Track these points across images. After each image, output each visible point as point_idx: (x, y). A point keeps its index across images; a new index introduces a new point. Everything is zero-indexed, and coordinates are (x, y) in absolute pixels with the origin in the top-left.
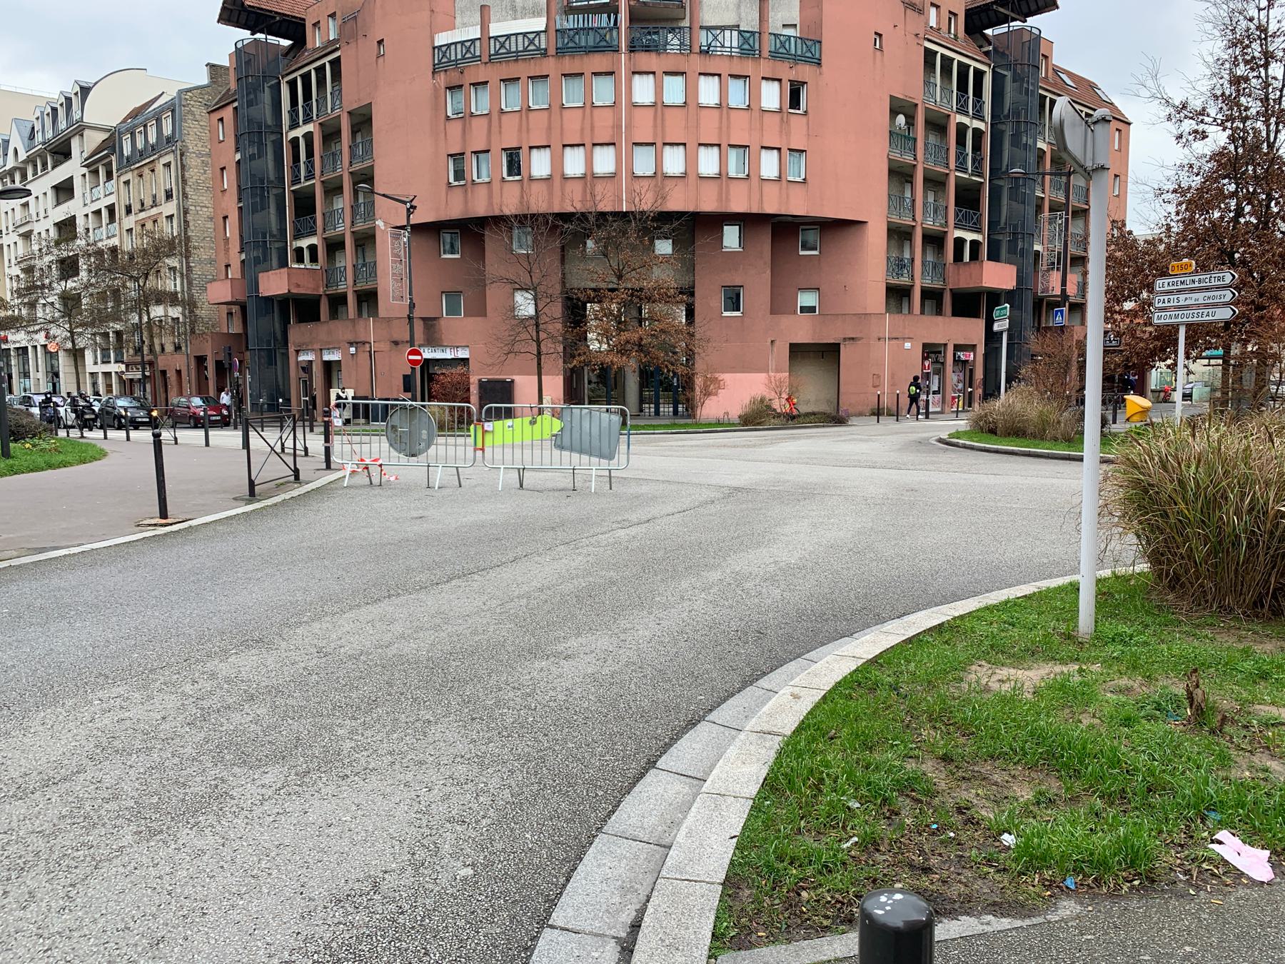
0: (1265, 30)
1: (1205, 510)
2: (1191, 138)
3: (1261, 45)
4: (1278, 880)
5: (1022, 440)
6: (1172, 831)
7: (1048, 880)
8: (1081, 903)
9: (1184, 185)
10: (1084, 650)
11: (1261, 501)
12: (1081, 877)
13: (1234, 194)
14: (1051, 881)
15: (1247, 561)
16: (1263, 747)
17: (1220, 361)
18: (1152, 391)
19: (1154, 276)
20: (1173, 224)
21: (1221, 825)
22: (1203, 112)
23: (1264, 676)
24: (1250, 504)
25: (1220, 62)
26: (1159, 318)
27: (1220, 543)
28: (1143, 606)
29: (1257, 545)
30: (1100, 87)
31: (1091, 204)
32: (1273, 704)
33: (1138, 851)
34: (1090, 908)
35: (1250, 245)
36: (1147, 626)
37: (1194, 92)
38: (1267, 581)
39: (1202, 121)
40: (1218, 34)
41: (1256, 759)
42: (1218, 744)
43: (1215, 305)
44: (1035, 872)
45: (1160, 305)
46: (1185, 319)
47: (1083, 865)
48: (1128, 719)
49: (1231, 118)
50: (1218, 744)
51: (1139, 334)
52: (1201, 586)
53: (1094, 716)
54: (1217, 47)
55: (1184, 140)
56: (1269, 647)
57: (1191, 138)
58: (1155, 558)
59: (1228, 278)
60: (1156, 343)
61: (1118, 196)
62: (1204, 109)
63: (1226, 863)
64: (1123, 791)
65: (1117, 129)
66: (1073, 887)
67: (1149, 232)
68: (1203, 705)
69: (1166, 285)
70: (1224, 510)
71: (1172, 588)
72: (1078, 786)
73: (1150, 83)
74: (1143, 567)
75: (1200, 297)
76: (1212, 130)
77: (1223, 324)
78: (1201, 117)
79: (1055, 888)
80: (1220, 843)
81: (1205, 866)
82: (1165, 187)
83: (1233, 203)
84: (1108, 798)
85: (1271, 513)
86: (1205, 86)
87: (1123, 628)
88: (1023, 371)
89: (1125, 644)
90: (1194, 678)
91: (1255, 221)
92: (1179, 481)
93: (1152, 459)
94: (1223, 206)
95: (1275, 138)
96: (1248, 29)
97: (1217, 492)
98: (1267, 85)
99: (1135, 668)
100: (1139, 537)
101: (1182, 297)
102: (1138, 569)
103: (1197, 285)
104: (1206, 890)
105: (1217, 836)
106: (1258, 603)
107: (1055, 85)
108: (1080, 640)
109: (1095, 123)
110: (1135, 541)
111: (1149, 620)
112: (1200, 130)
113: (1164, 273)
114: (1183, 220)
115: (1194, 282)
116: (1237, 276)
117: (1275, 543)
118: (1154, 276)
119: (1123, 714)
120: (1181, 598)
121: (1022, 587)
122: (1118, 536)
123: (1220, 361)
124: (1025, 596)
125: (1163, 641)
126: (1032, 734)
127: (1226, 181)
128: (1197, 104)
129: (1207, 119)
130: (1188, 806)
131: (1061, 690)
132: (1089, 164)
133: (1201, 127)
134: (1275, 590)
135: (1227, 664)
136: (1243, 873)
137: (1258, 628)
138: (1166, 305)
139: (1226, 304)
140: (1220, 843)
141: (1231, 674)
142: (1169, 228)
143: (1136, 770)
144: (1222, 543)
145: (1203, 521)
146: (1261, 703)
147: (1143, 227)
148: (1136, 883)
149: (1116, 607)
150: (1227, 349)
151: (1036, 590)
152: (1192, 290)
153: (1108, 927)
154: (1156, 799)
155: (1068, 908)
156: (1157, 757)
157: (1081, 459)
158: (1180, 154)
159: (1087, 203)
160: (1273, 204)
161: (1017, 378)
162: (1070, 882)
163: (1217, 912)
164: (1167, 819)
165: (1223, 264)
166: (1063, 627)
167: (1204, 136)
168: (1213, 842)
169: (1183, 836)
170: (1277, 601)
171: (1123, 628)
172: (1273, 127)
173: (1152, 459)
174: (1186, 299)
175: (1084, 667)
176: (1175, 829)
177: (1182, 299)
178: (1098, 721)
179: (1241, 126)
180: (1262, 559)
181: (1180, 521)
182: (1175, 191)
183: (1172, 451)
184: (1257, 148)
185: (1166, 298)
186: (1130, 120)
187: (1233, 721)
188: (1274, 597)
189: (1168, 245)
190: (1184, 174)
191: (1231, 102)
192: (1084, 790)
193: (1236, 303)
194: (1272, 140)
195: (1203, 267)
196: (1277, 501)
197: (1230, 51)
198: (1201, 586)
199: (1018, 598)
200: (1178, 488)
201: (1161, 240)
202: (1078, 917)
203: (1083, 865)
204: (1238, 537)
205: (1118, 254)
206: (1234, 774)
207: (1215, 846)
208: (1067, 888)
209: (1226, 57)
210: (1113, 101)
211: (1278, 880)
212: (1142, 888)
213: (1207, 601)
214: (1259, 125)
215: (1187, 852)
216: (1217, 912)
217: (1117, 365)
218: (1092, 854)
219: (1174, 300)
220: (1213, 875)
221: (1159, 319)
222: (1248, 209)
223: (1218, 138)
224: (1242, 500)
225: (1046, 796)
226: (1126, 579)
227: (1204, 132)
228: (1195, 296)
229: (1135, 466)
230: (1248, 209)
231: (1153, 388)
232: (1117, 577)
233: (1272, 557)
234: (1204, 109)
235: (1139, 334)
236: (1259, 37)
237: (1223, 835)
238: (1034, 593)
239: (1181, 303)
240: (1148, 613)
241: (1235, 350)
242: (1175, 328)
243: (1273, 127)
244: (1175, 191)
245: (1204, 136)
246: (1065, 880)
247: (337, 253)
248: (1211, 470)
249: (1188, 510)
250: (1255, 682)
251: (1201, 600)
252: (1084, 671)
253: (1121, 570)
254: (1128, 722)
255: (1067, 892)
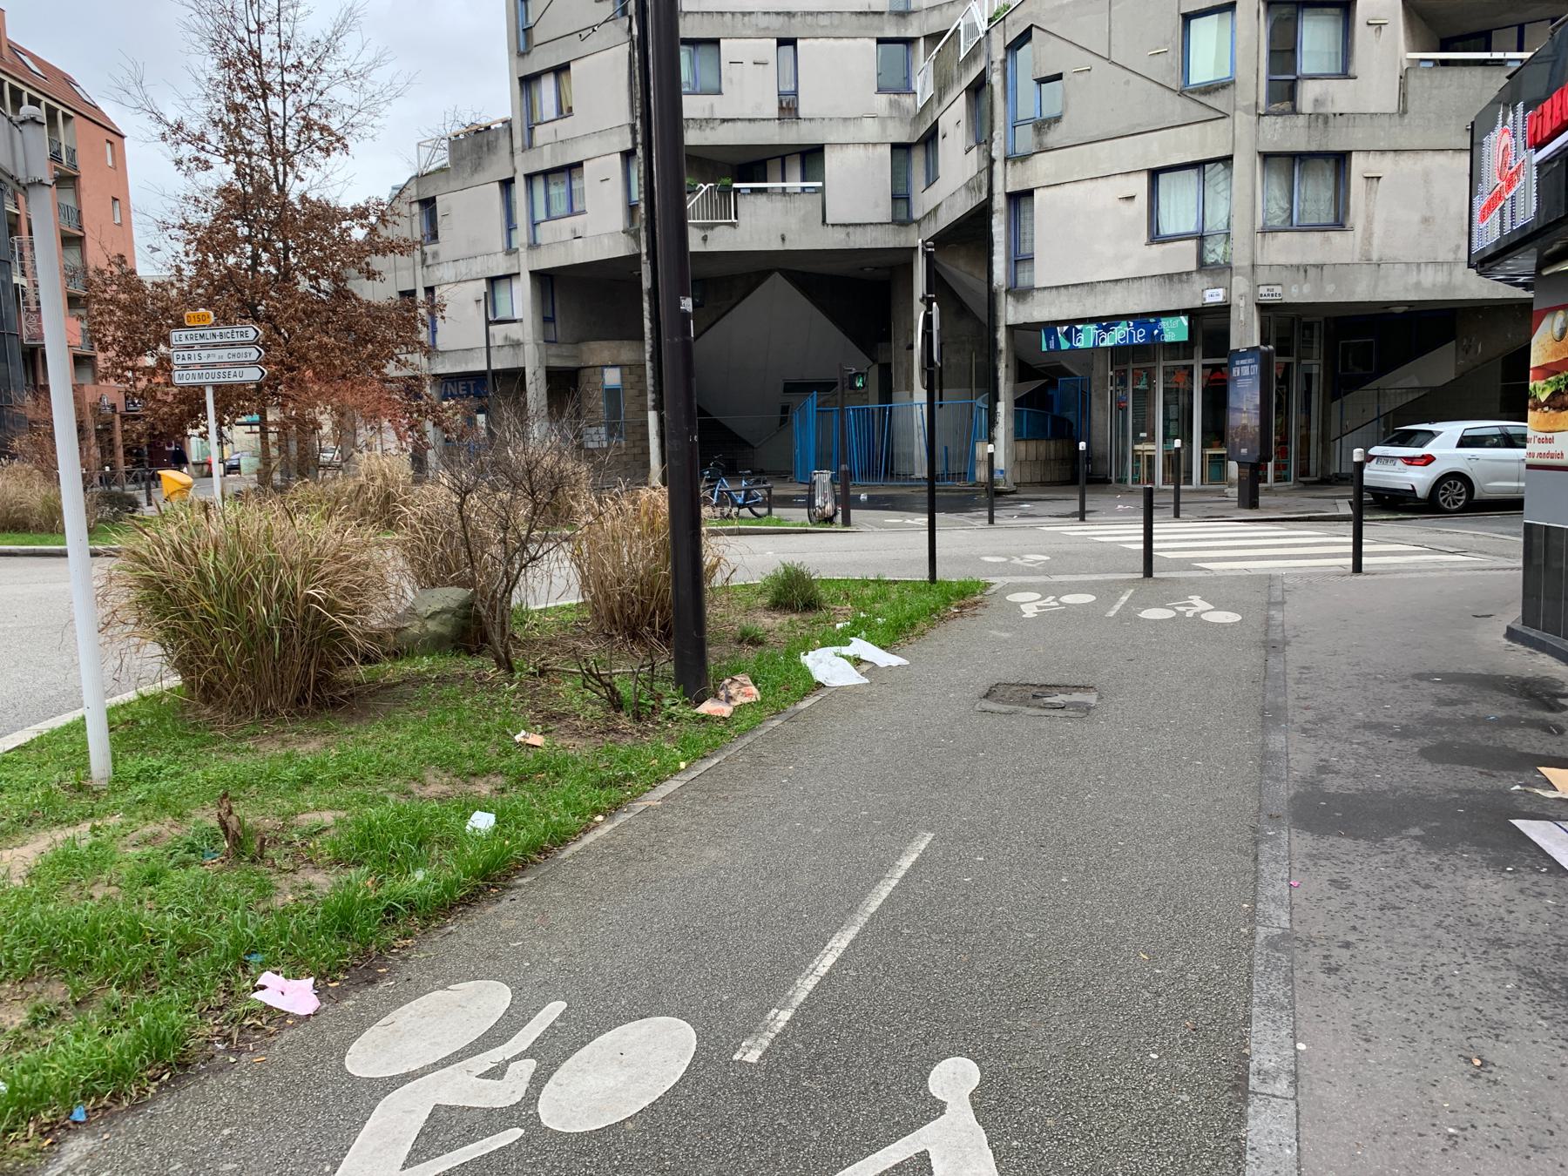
0: (259, 57)
1: (231, 603)
2: (193, 165)
3: (256, 73)
4: (325, 1005)
5: (25, 535)
6: (209, 995)
7: (47, 1124)
8: (94, 1135)
9: (193, 220)
10: (102, 799)
11: (289, 586)
12: (93, 1100)
13: (248, 239)
14: (52, 1123)
15: (283, 655)
16: (306, 862)
17: (257, 428)
18: (194, 464)
19: (169, 327)
20: (183, 266)
21: (264, 966)
22: (202, 138)
23: (308, 780)
24: (278, 590)
25: (214, 83)
26: (181, 377)
27: (253, 638)
28: (175, 728)
29: (292, 635)
30: (78, 82)
31: (86, 229)
32: (317, 809)
33: (164, 1038)
34: (106, 1136)
35: (272, 298)
36: (179, 753)
37: (190, 113)
38: (308, 673)
39: (203, 148)
40: (206, 48)
41: (298, 878)
42: (258, 874)
43: (242, 364)
44: (29, 1122)
45: (180, 362)
46: (210, 380)
47: (94, 1084)
48: (152, 875)
49: (236, 152)
50: (258, 874)
51: (159, 395)
52: (239, 691)
53: (109, 884)
54: (209, 65)
55: (185, 168)
56: (313, 745)
57: (193, 165)
58: (183, 666)
59: (252, 334)
60: (183, 407)
61: (119, 225)
62: (203, 134)
63: (269, 1008)
64: (150, 967)
65: (108, 141)
66: (82, 1118)
67: (155, 273)
68: (239, 833)
69: (183, 338)
70: (252, 600)
71: (208, 701)
72: (88, 982)
73: (134, 90)
74: (175, 681)
75: (223, 355)
76: (216, 160)
77: (254, 386)
78: (201, 144)
79: (58, 1130)
80: (263, 988)
81: (247, 1022)
82: (171, 221)
83: (248, 248)
84: (130, 984)
85: (300, 597)
86: (201, 107)
87: (150, 761)
88: (16, 444)
89: (153, 780)
90: (225, 805)
91: (275, 272)
92: (199, 573)
93: (162, 549)
94: (238, 250)
95: (285, 181)
96: (240, 51)
97: (242, 581)
98: (267, 119)
99: (164, 807)
100: (163, 645)
101: (204, 353)
102: (166, 684)
103: (218, 339)
104: (248, 1051)
105: (260, 982)
106: (300, 700)
107: (14, 67)
108: (95, 789)
109: (22, 122)
110: (160, 651)
111: (181, 744)
112: (202, 158)
113: (180, 324)
114: (195, 263)
115: (214, 336)
116: (261, 332)
117: (309, 631)
118: (169, 327)
119: (147, 869)
120: (219, 709)
121: (15, 735)
122: (133, 649)
123: (257, 428)
124: (18, 747)
125: (198, 766)
126: (21, 934)
127: (238, 222)
128: (194, 127)
129: (208, 147)
130: (226, 958)
131: (68, 866)
132: (21, 176)
133: (203, 155)
134: (316, 682)
135: (269, 776)
136: (288, 1014)
137: (302, 727)
138: (187, 362)
139: (253, 364)
140: (263, 988)
141: (274, 787)
142: (179, 270)
143: (164, 935)
144: (256, 639)
145: (231, 617)
146: (307, 810)
147: (147, 266)
148: (166, 1077)
149: (142, 737)
150: (263, 414)
151: (34, 736)
152: (216, 346)
153: (130, 1149)
154: (189, 964)
155: (77, 1148)
156: (188, 911)
157: (65, 555)
158: (179, 183)
159: (81, 228)
160: (291, 255)
161: (8, 453)
162: (79, 1114)
163: (260, 1073)
164: (202, 983)
165: (246, 318)
166: (70, 778)
167: (207, 166)
168: (255, 990)
169: (222, 995)
170: (321, 693)
171: (150, 761)
172: (280, 168)
173: (162, 549)
174: (209, 356)
175: (98, 823)
176: (212, 992)
177: (206, 356)
178: (116, 889)
179: (246, 161)
180: (298, 649)
181: (204, 620)
182: (182, 227)
183: (186, 538)
184: (267, 189)
185: (186, 354)
186: (123, 132)
187: (276, 841)
188: (317, 689)
189: (181, 290)
190: (190, 207)
191: (232, 132)
192: (98, 984)
193: (267, 364)
194: (281, 182)
195: (224, 319)
196: (305, 583)
197: (222, 72)
198: (239, 691)
199: (9, 752)
200: (198, 582)
201: (172, 285)
202: (90, 1155)
203: (94, 1084)
204: (270, 631)
205: (122, 296)
206: (277, 902)
207: (258, 995)
208: (75, 1122)
209: (220, 78)
210: (98, 104)
211: (325, 1005)
212: (174, 1081)
213: (247, 708)
214: (266, 164)
215: (226, 1014)
216: (260, 1073)
217: (140, 435)
218: (105, 1066)
219: (194, 357)
220: (257, 1029)
221: (181, 378)
222: (265, 256)
223: (223, 172)
224: (270, 588)
225: (45, 1012)
226: (157, 698)
227: (206, 162)
228: (218, 352)
229: (143, 560)
230: (265, 256)
231: (195, 460)
232: (144, 698)
233: (308, 645)
234: (203, 134)
235: (159, 395)
236: (254, 64)
237: (267, 978)
238: (32, 741)
239: (204, 360)
240: (181, 736)
241: (273, 416)
242: (201, 389)
243: (280, 168)
244: (182, 227)
245: (207, 166)
246: (71, 1114)
247: (1022, 204)
248: (231, 557)
249: (212, 606)
250: (299, 790)
251: (241, 709)
252: (98, 828)
253: (147, 690)
254: (152, 879)
255: (74, 1128)
